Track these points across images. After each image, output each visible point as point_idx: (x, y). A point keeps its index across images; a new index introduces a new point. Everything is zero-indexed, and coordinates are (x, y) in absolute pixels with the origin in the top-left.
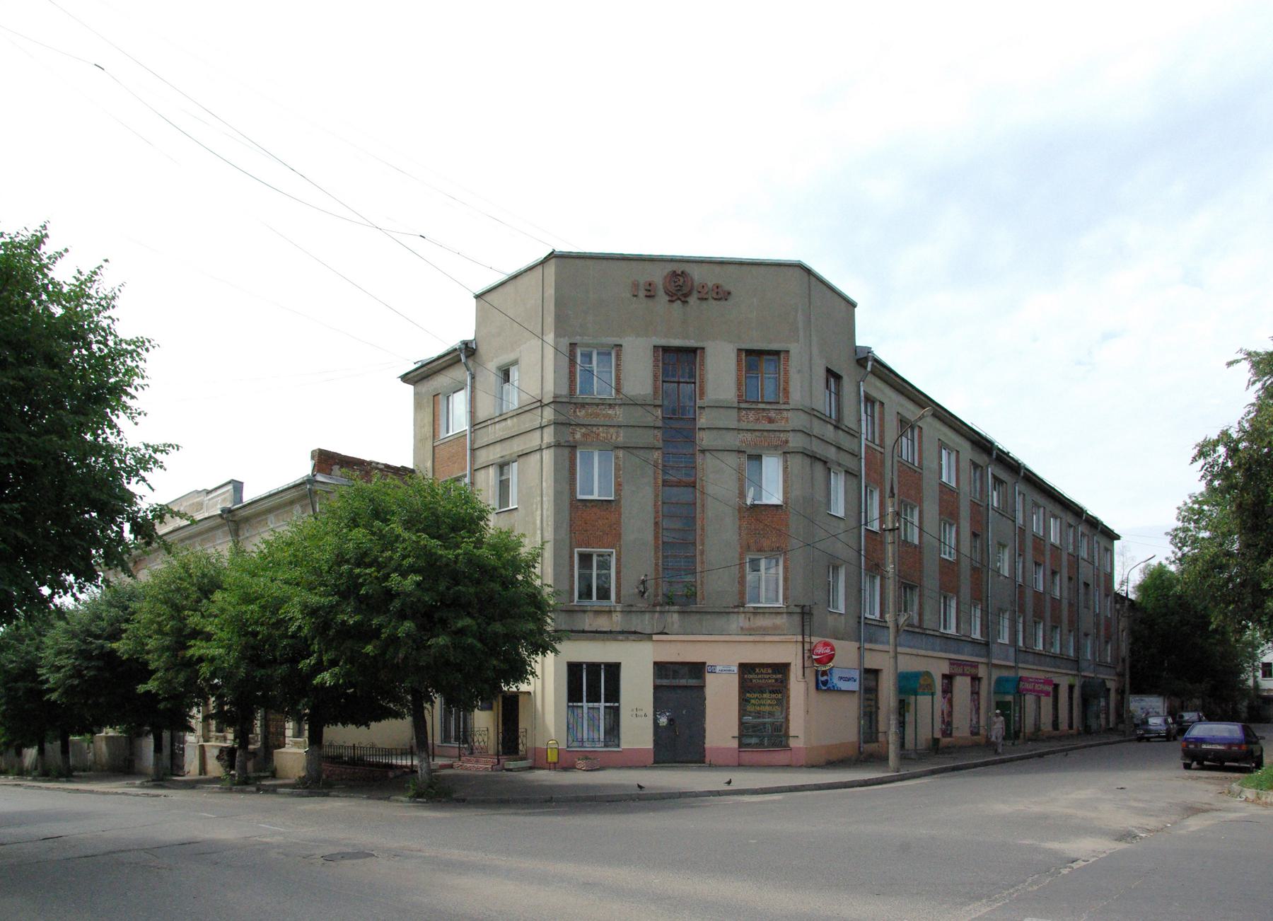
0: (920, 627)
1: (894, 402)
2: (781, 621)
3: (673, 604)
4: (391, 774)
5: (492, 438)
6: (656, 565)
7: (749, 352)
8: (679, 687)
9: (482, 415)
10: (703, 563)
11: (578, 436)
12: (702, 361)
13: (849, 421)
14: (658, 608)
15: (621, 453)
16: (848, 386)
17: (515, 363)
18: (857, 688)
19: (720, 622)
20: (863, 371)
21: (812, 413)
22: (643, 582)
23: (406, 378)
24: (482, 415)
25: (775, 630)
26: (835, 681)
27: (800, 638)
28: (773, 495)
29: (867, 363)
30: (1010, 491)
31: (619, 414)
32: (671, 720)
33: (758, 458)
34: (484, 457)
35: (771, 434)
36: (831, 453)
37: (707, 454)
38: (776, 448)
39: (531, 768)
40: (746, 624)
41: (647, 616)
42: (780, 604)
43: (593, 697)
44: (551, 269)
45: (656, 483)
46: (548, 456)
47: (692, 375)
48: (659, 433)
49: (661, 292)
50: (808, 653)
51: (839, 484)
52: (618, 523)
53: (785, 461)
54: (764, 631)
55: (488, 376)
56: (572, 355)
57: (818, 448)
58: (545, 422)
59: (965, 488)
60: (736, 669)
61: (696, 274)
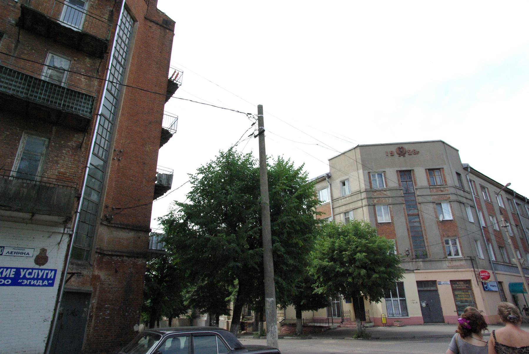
0: (510, 263)
1: (478, 181)
2: (463, 263)
3: (419, 258)
4: (323, 330)
5: (341, 204)
6: (410, 244)
7: (429, 170)
8: (427, 291)
9: (335, 197)
10: (427, 242)
11: (375, 201)
12: (414, 175)
13: (467, 189)
14: (414, 260)
15: (391, 206)
16: (463, 176)
17: (348, 179)
18: (497, 290)
19: (439, 264)
20: (467, 172)
21: (455, 187)
22: (408, 250)
24: (335, 197)
25: (461, 267)
26: (489, 286)
27: (472, 269)
28: (448, 216)
29: (467, 168)
30: (523, 208)
31: (388, 193)
32: (427, 304)
33: (440, 204)
34: (337, 211)
35: (443, 196)
36: (464, 200)
37: (422, 205)
38: (446, 200)
39: (374, 326)
40: (450, 265)
41: (410, 263)
42: (461, 256)
43: (395, 295)
44: (358, 150)
45: (405, 215)
46: (366, 209)
47: (410, 178)
48: (403, 198)
49: (395, 154)
50: (477, 276)
51: (469, 211)
52: (394, 230)
53: (451, 205)
54: (457, 267)
55: (337, 183)
56: (369, 176)
57: (461, 199)
58: (363, 197)
59: (508, 208)
60: (449, 282)
61: (406, 147)
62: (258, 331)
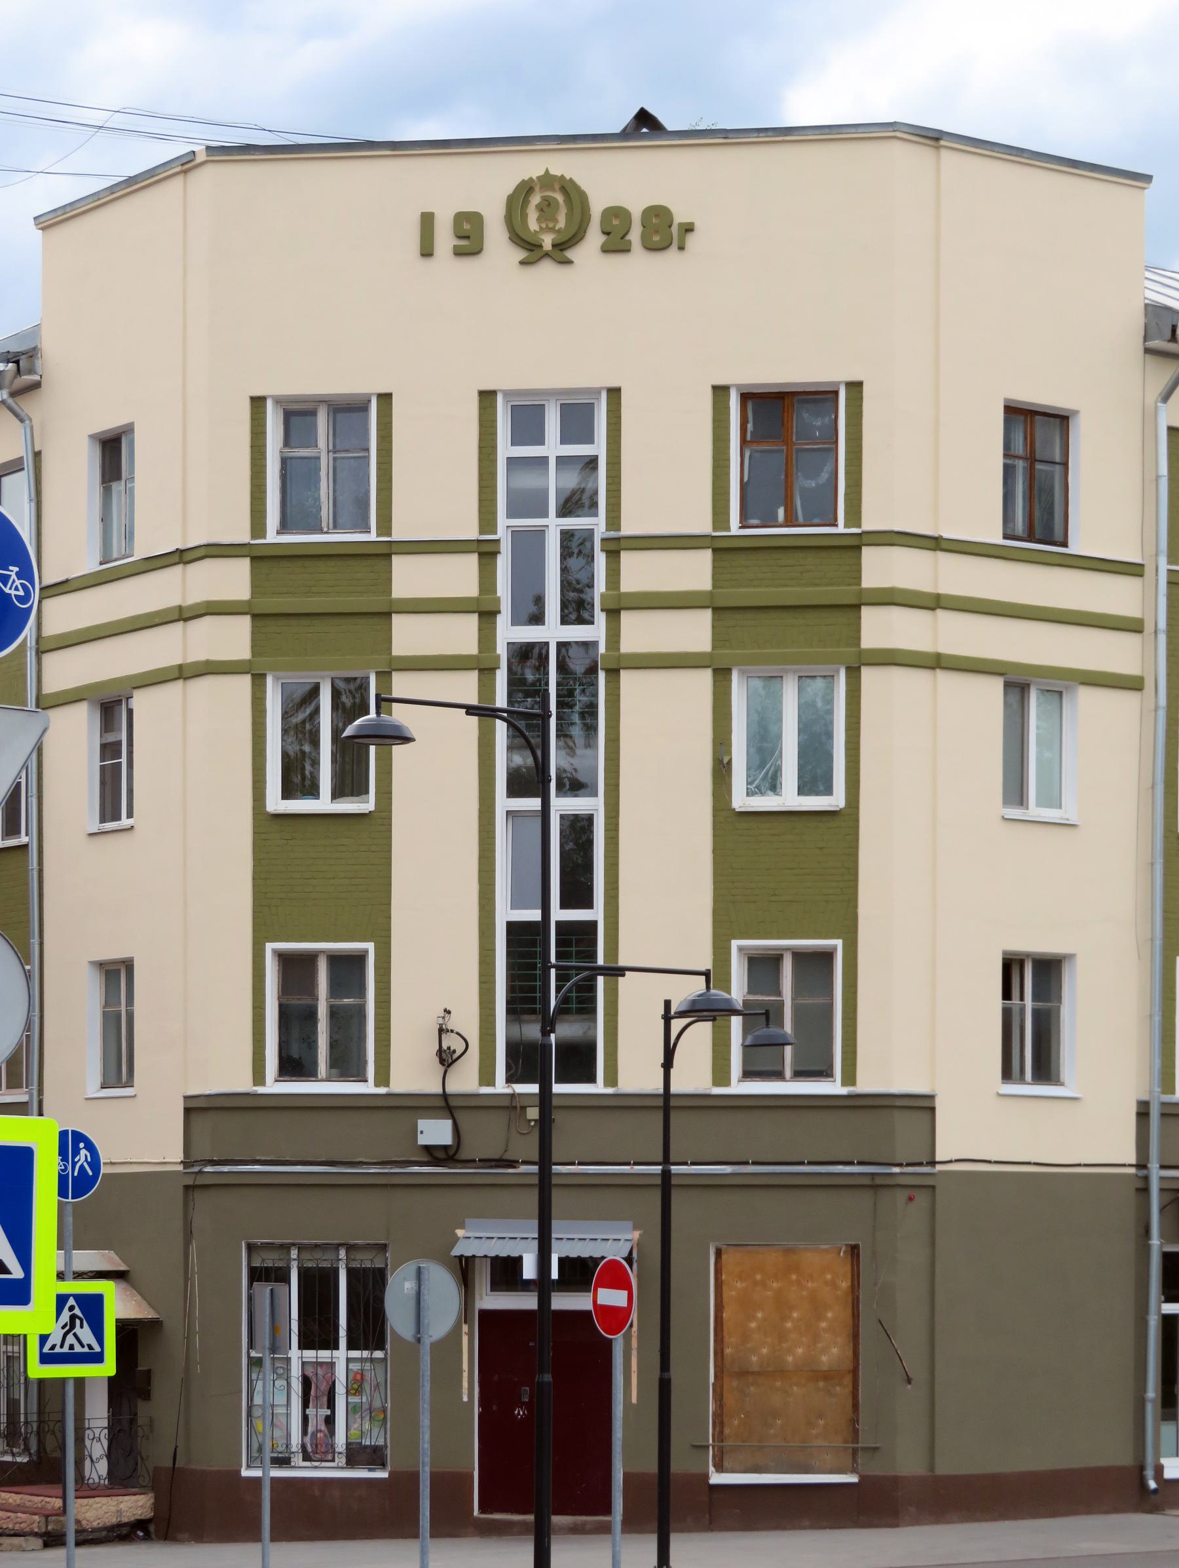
23: (547, 170)
62: (432, 1344)
